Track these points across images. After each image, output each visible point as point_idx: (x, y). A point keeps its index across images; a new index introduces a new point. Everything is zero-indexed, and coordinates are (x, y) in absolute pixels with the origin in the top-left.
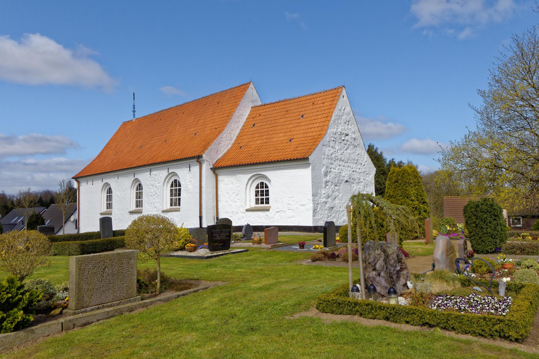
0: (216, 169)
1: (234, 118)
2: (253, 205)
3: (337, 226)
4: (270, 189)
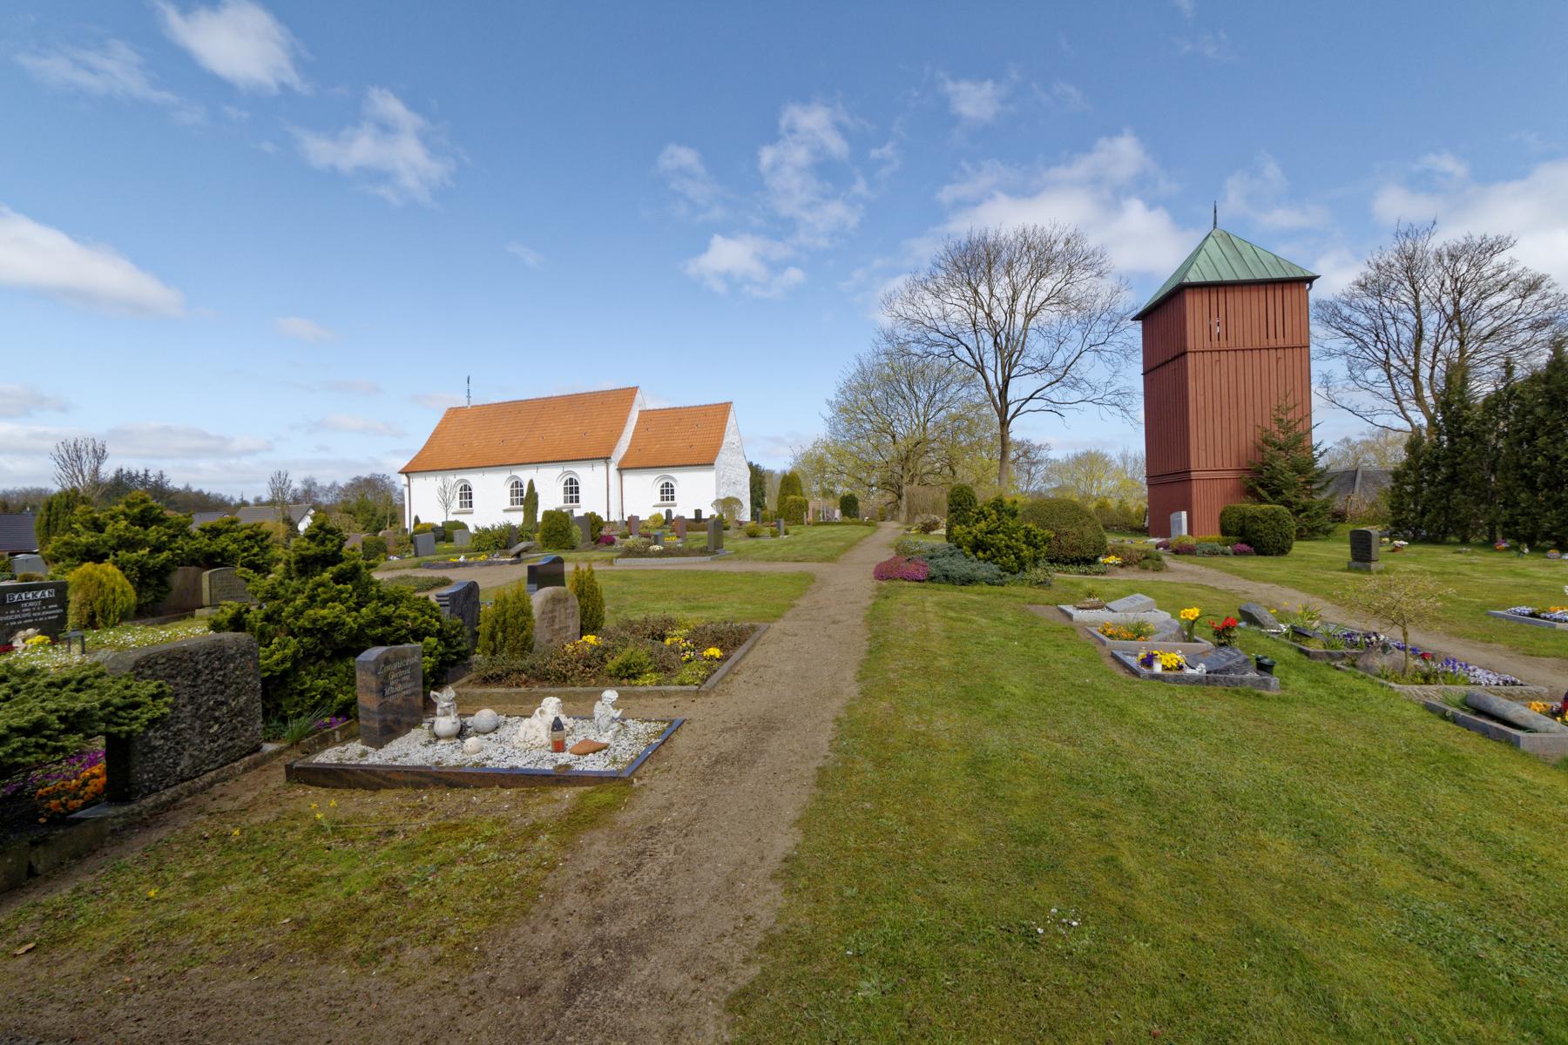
0: (621, 470)
1: (629, 422)
2: (508, 505)
3: (1169, 519)
4: (675, 488)
